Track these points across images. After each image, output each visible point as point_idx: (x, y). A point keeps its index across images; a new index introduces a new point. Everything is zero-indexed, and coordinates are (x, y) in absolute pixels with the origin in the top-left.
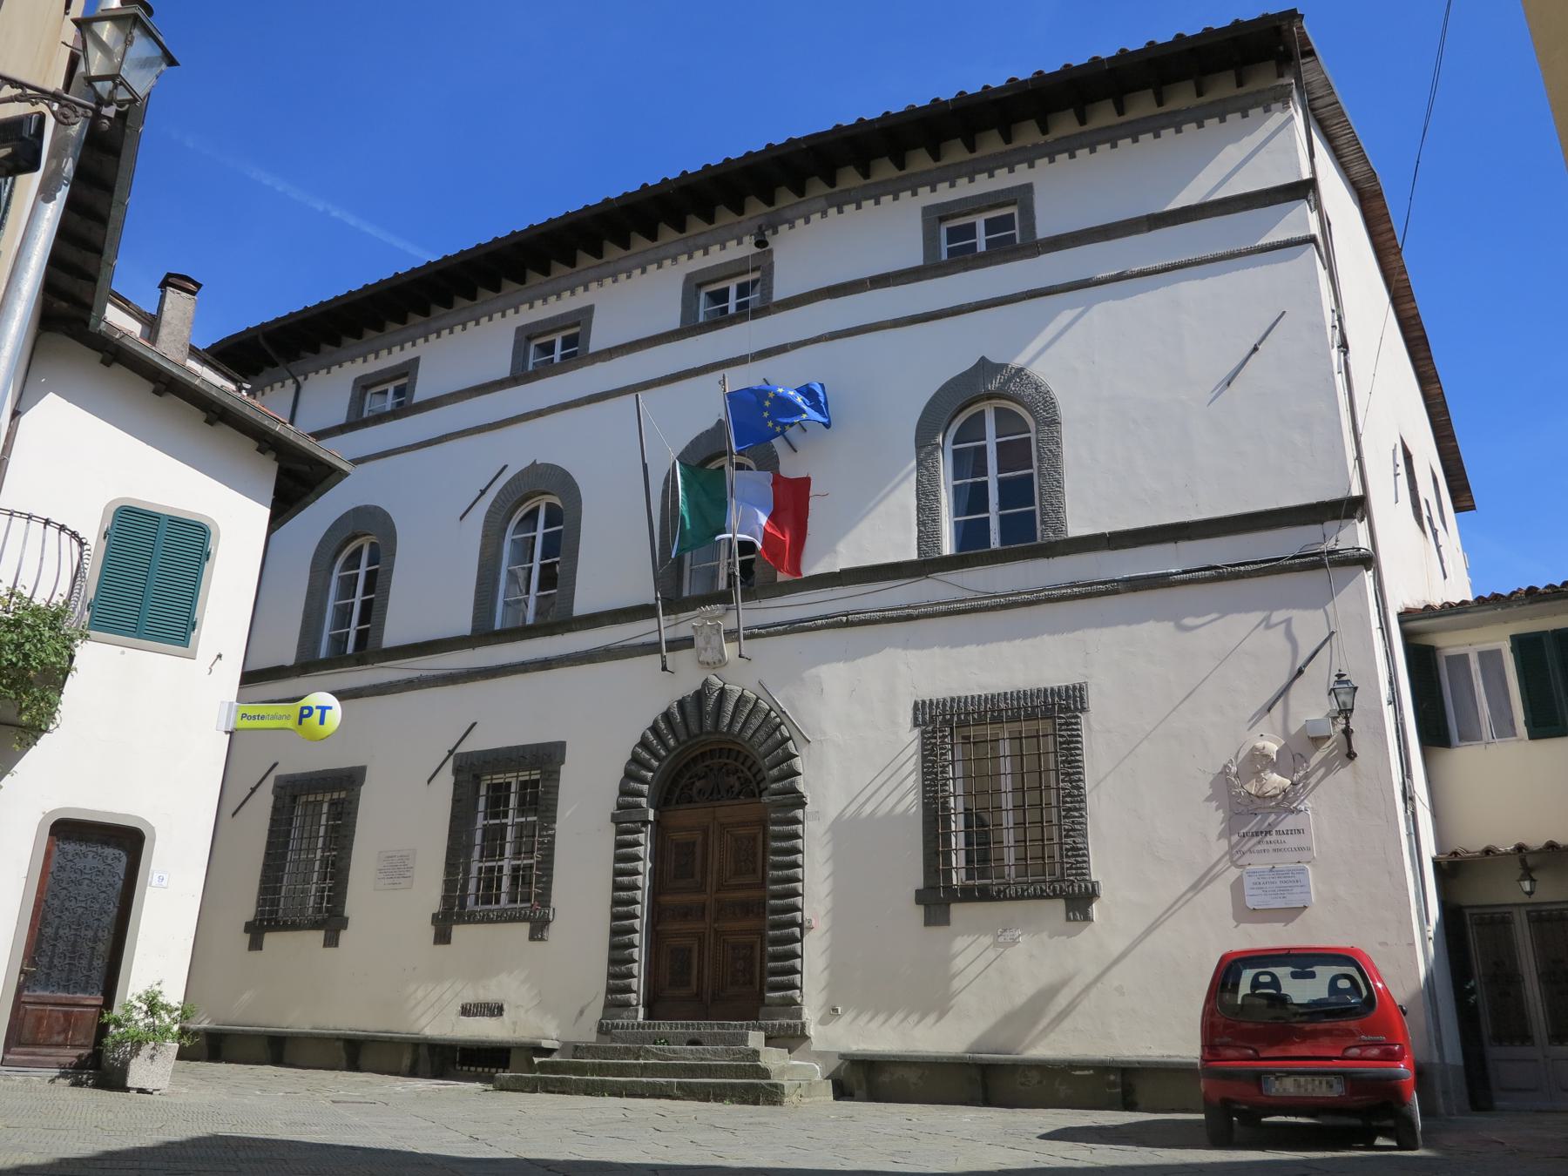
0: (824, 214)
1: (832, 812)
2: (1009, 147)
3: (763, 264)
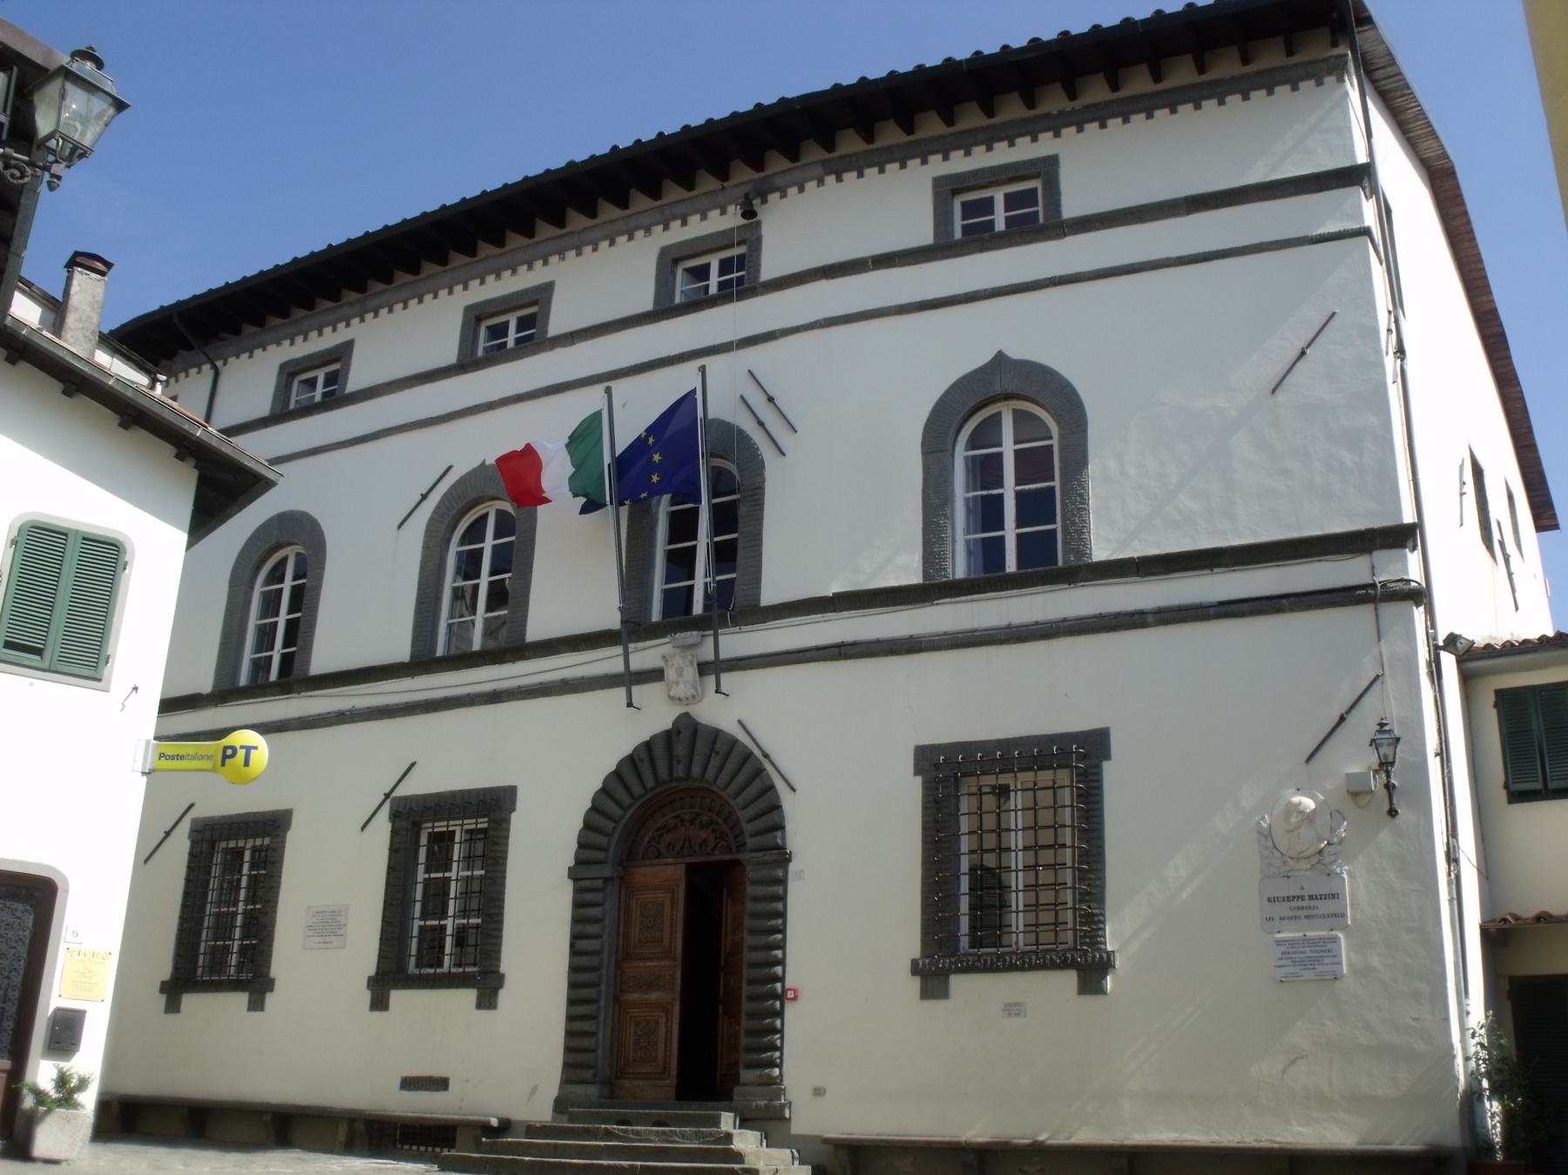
0: (821, 182)
2: (1032, 113)
3: (750, 236)
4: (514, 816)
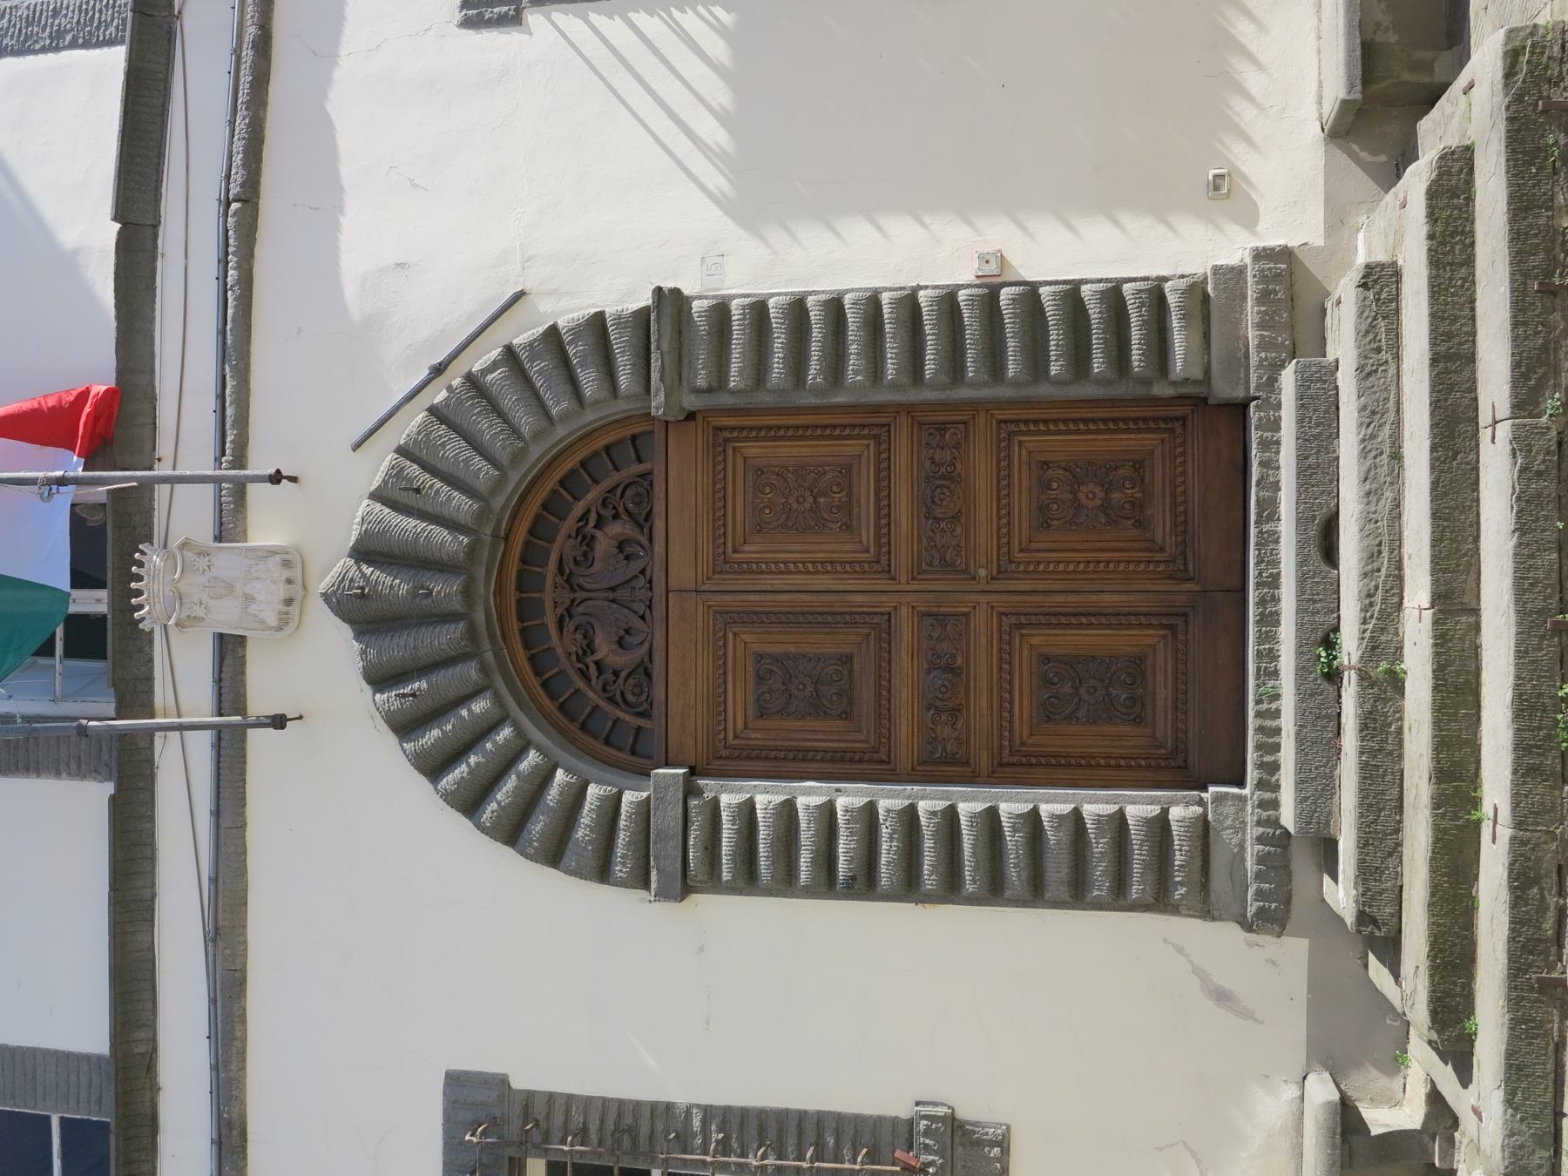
1: (713, 221)
4: (520, 1082)
